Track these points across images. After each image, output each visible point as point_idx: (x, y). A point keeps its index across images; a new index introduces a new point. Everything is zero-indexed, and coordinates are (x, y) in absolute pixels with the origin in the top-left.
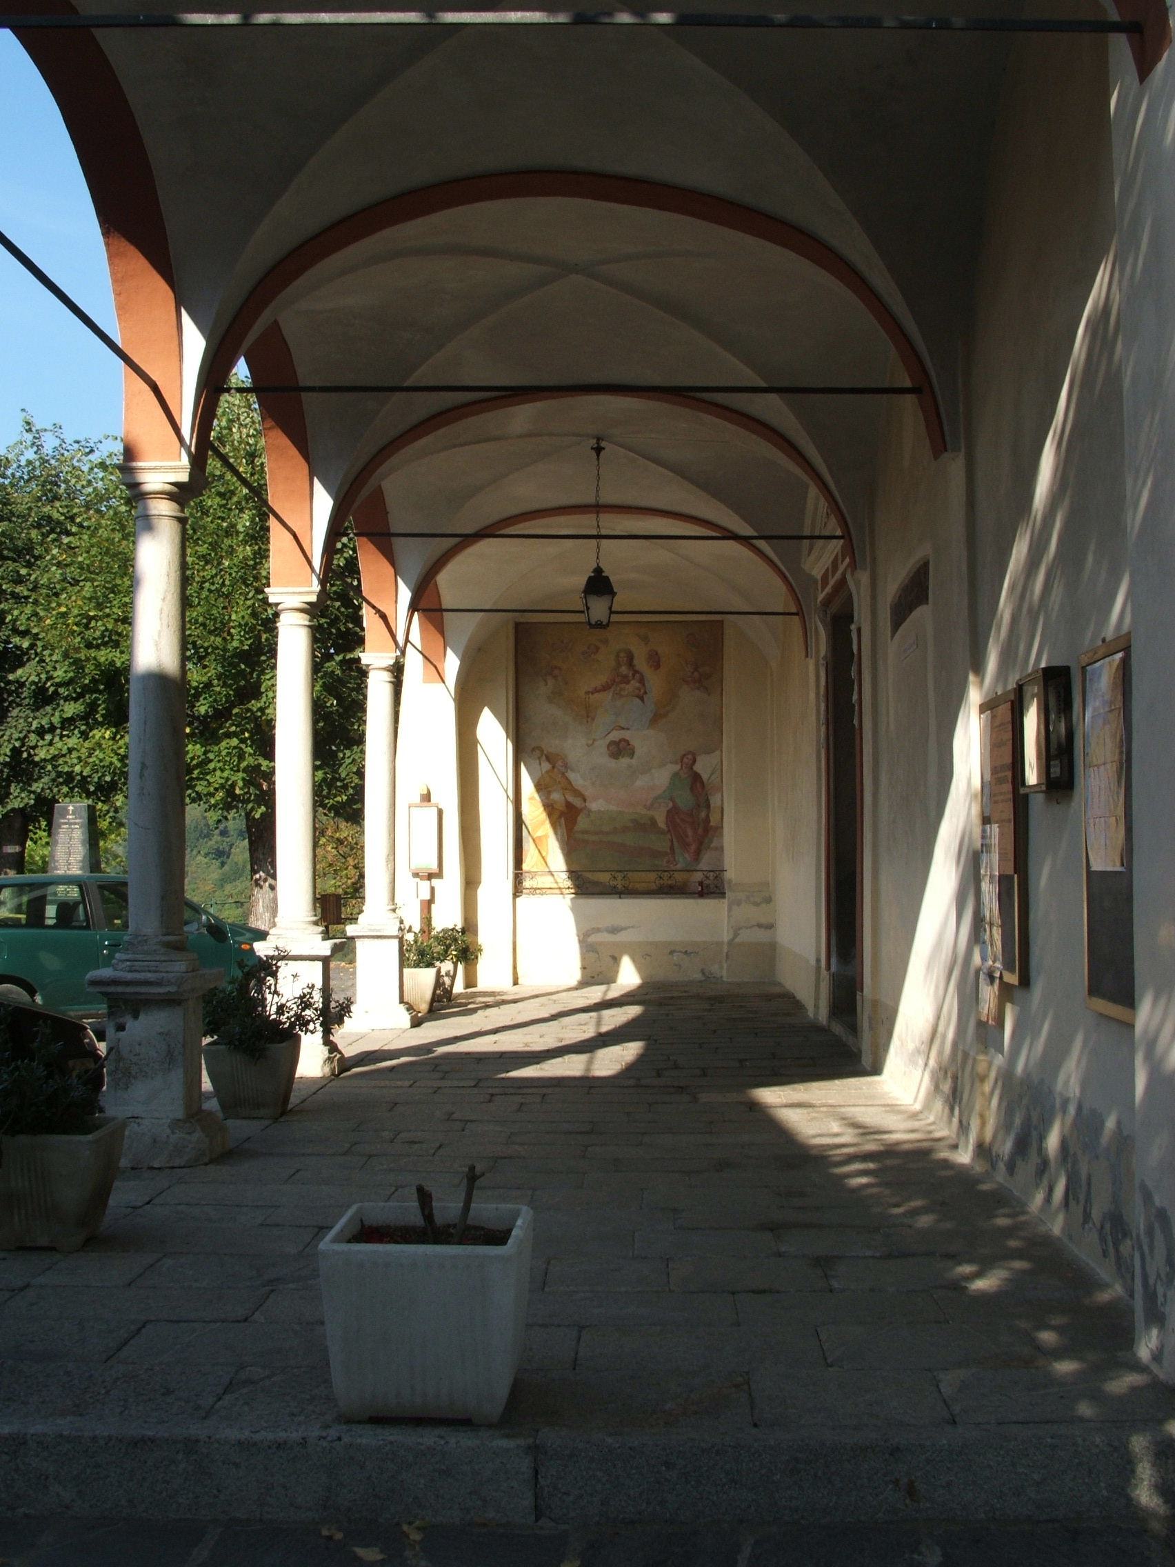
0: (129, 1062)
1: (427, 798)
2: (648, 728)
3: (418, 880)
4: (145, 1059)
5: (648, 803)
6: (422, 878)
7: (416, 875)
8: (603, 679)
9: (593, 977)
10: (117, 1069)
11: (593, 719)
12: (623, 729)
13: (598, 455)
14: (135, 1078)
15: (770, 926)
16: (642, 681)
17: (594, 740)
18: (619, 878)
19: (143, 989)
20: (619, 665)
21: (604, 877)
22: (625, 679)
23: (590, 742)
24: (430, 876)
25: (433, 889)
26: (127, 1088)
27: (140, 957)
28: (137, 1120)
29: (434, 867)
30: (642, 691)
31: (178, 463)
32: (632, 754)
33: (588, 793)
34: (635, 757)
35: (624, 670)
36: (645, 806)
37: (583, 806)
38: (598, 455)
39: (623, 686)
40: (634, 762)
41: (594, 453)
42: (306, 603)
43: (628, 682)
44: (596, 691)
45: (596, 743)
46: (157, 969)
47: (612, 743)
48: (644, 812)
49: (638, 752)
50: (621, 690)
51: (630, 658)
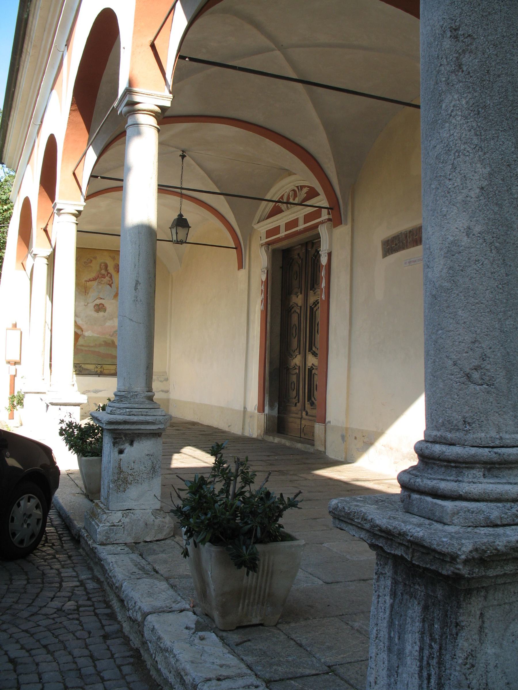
0: (126, 474)
1: (15, 326)
2: (113, 299)
3: (9, 365)
4: (137, 472)
5: (111, 333)
6: (11, 364)
7: (9, 362)
8: (93, 275)
9: (86, 413)
10: (118, 479)
11: (88, 294)
12: (102, 299)
13: (183, 159)
14: (131, 484)
15: (167, 392)
16: (111, 277)
17: (88, 303)
18: (99, 367)
19: (142, 427)
20: (101, 269)
21: (91, 367)
22: (104, 276)
23: (86, 304)
24: (16, 363)
25: (16, 370)
26: (124, 491)
27: (136, 406)
28: (131, 511)
29: (17, 359)
30: (111, 282)
31: (162, 94)
32: (105, 310)
33: (84, 327)
34: (107, 311)
35: (103, 272)
36: (110, 335)
37: (81, 333)
38: (183, 159)
39: (103, 279)
40: (106, 314)
41: (180, 158)
42: (77, 211)
43: (105, 278)
44: (90, 280)
45: (89, 305)
46: (147, 414)
47: (96, 305)
48: (109, 337)
49: (108, 310)
50: (102, 281)
51: (106, 266)
